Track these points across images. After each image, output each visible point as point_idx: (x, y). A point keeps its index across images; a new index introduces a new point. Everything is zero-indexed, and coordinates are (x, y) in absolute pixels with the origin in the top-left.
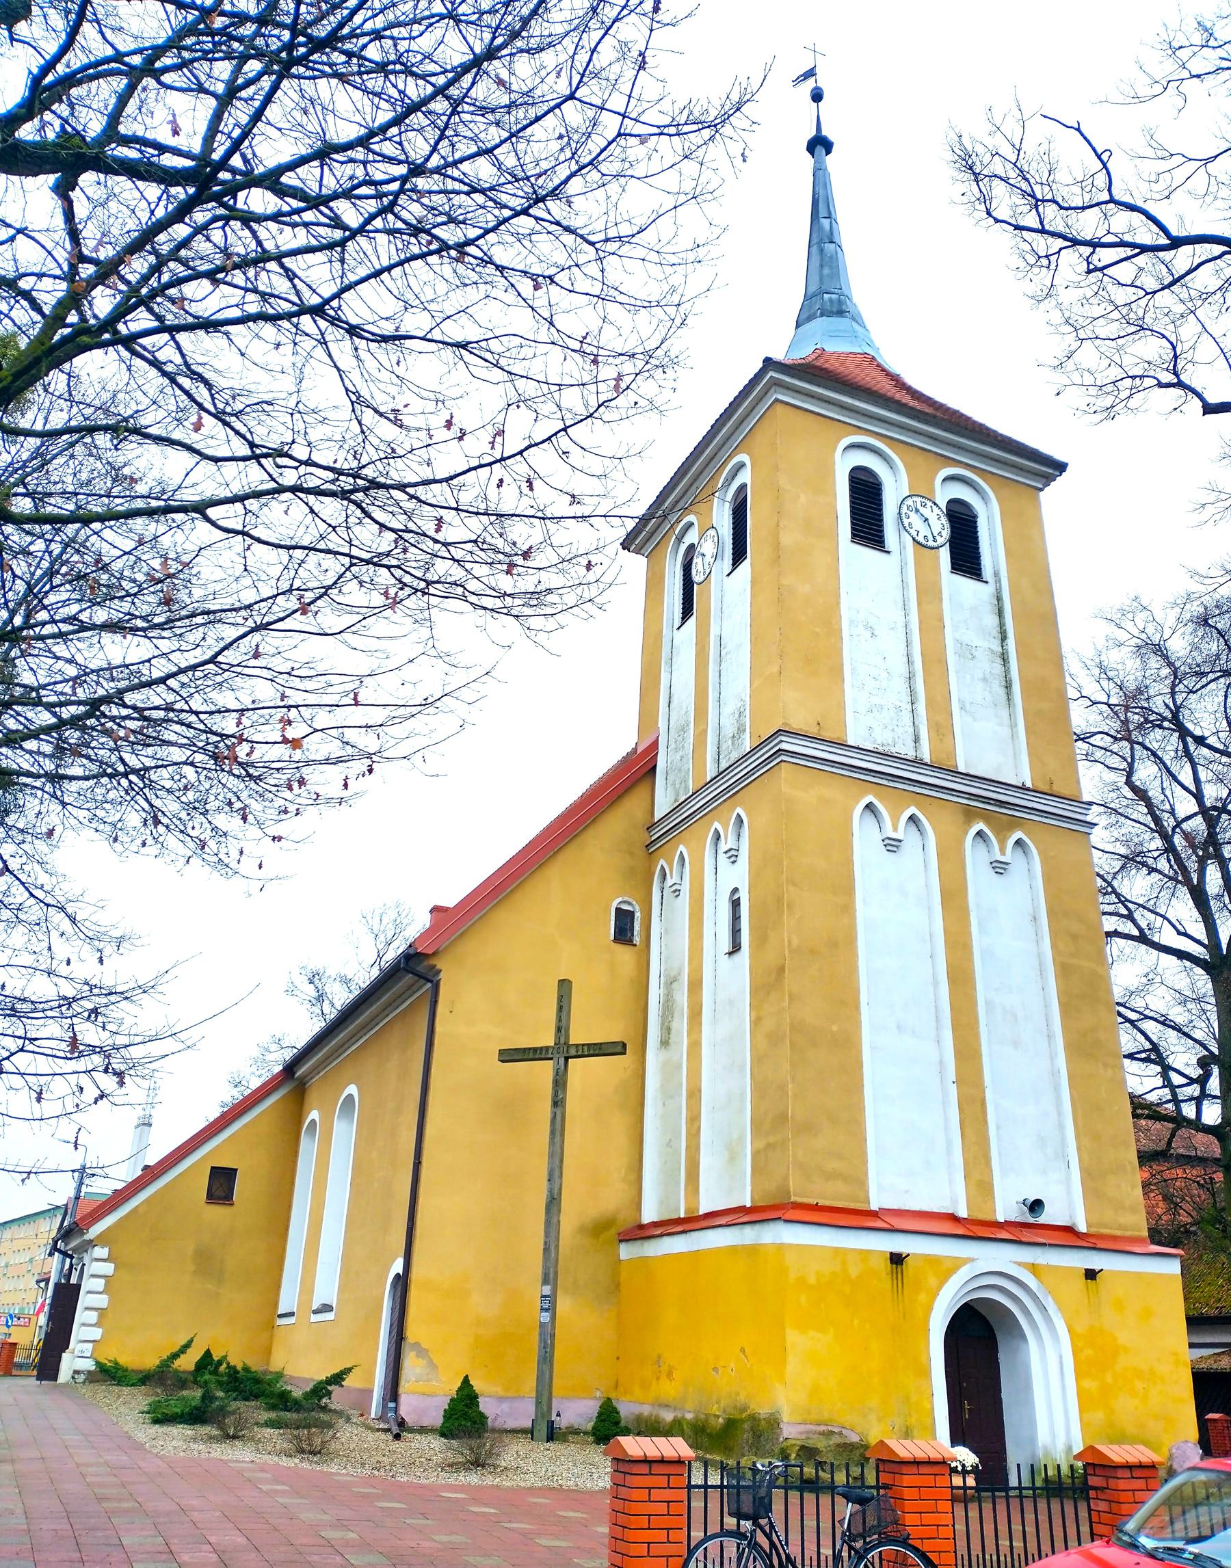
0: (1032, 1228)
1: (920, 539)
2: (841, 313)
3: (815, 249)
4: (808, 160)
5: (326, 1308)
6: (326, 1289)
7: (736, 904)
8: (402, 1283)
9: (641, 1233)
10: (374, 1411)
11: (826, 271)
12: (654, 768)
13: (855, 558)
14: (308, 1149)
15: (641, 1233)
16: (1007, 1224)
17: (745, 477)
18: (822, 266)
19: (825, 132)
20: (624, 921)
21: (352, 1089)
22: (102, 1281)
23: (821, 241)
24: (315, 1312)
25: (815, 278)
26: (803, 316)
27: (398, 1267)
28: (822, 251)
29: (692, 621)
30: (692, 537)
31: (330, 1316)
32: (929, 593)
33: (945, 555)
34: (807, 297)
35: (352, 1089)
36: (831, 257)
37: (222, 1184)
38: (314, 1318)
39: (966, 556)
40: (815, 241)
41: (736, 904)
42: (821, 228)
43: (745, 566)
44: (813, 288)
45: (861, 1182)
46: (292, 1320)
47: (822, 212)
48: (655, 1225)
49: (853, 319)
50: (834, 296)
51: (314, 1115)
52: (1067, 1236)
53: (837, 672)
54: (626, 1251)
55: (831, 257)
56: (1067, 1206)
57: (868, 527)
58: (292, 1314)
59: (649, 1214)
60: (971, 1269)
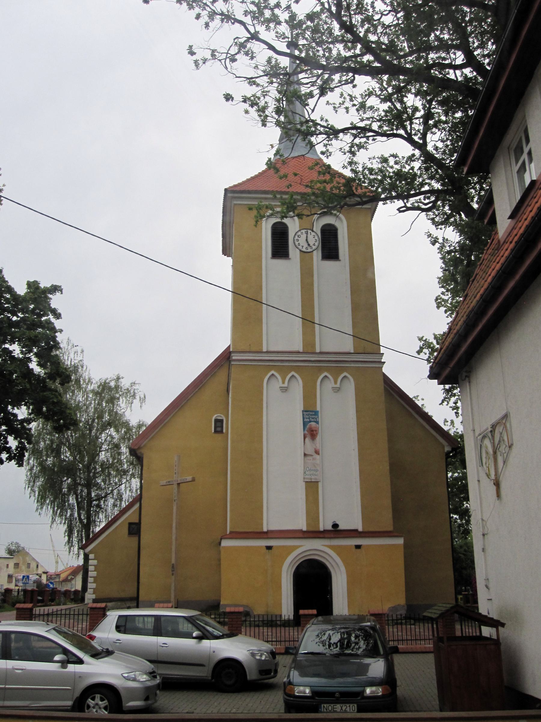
0: (335, 531)
1: (304, 250)
16: (325, 531)
20: (219, 423)
33: (317, 255)
52: (353, 533)
57: (280, 249)
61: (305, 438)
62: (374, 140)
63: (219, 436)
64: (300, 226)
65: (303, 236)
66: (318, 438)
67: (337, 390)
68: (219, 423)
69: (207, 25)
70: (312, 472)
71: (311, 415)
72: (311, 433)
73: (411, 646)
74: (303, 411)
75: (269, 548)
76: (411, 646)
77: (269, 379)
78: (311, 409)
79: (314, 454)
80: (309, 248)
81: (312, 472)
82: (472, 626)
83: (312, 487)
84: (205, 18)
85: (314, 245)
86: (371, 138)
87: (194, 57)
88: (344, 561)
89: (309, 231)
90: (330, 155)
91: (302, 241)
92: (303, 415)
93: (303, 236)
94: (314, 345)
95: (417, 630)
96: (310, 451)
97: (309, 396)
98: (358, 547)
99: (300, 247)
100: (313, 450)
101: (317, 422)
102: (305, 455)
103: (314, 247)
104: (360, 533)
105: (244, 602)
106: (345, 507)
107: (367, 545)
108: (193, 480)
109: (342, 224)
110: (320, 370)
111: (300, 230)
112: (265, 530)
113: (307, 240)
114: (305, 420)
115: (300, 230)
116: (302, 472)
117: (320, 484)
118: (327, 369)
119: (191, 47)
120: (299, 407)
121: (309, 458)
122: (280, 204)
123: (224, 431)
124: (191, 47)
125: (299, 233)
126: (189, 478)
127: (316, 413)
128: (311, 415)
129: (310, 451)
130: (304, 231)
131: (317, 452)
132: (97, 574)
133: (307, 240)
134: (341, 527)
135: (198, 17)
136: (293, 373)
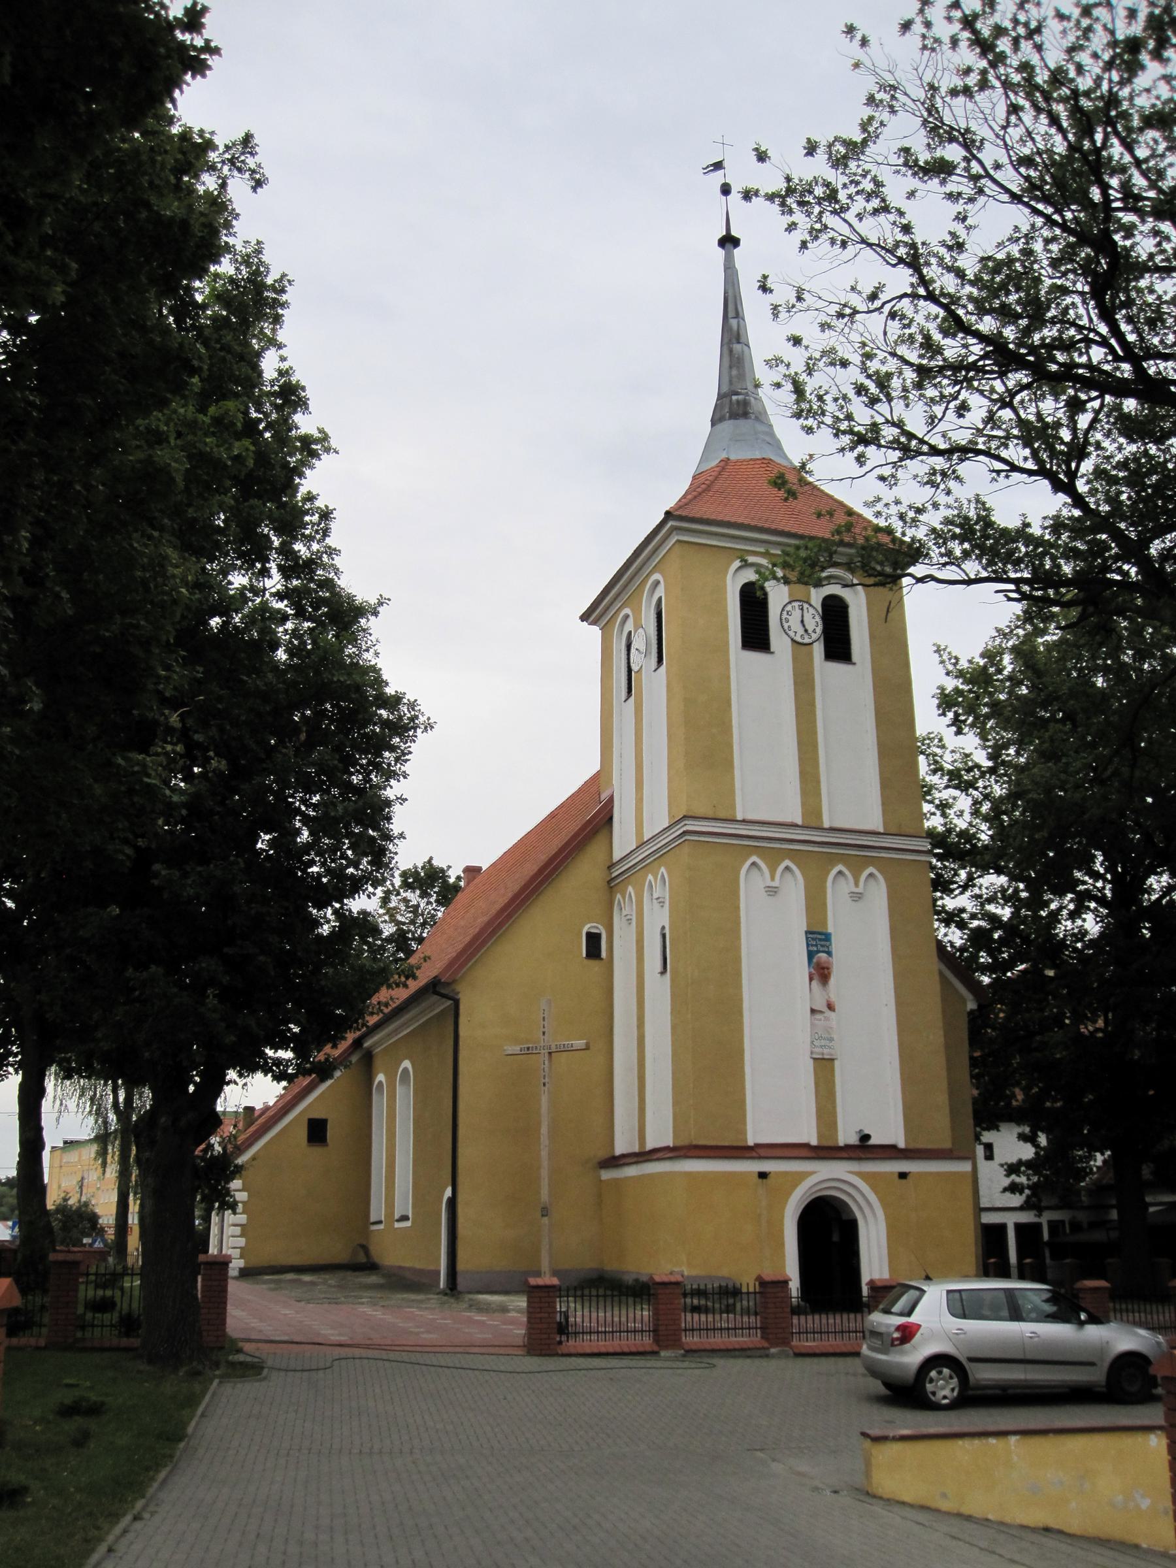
0: (863, 1149)
1: (798, 639)
2: (745, 415)
3: (725, 347)
4: (721, 253)
5: (404, 1218)
6: (404, 1202)
7: (664, 936)
8: (452, 1203)
9: (614, 1162)
10: (442, 1285)
11: (734, 372)
12: (611, 818)
13: (742, 661)
14: (380, 1104)
15: (614, 1162)
16: (848, 1147)
17: (660, 592)
18: (731, 367)
19: (734, 233)
20: (593, 940)
21: (407, 1064)
22: (239, 1228)
23: (730, 342)
24: (398, 1221)
25: (726, 380)
26: (717, 417)
27: (448, 1192)
28: (731, 351)
29: (632, 698)
30: (629, 626)
31: (408, 1224)
32: (804, 684)
33: (818, 650)
34: (721, 396)
35: (407, 1064)
36: (738, 358)
37: (317, 1131)
38: (397, 1225)
39: (838, 646)
40: (726, 340)
41: (664, 936)
42: (731, 329)
43: (663, 668)
44: (725, 389)
45: (744, 1132)
46: (381, 1227)
47: (731, 314)
48: (623, 1156)
49: (757, 419)
50: (740, 397)
51: (381, 1077)
52: (890, 1152)
53: (729, 764)
54: (606, 1175)
55: (738, 358)
56: (889, 1129)
57: (756, 636)
58: (380, 1222)
59: (618, 1151)
60: (822, 1176)
61: (811, 979)
62: (1007, 477)
63: (593, 963)
64: (790, 595)
65: (793, 614)
66: (832, 981)
67: (857, 897)
68: (593, 940)
69: (804, 245)
70: (823, 1042)
71: (820, 940)
72: (821, 973)
73: (826, 1343)
74: (807, 933)
75: (763, 1175)
76: (826, 1343)
77: (748, 871)
78: (820, 930)
79: (825, 1009)
80: (806, 637)
81: (823, 1042)
82: (1158, 1312)
83: (824, 1066)
84: (800, 235)
85: (814, 631)
86: (1003, 474)
87: (769, 298)
88: (881, 1200)
89: (806, 606)
90: (895, 484)
91: (794, 622)
92: (807, 938)
93: (793, 614)
94: (819, 815)
95: (624, 1319)
96: (820, 1005)
97: (815, 903)
98: (903, 1176)
99: (792, 634)
100: (825, 1003)
101: (829, 953)
102: (813, 1011)
103: (815, 636)
104: (816, 1148)
105: (725, 1272)
106: (876, 1105)
107: (918, 1173)
108: (587, 1048)
109: (858, 603)
110: (833, 859)
111: (790, 603)
112: (750, 1143)
113: (802, 621)
114: (811, 948)
115: (790, 603)
116: (809, 1040)
117: (836, 1063)
118: (756, 850)
119: (765, 277)
120: (799, 925)
121: (818, 1016)
122: (779, 552)
123: (604, 954)
124: (765, 277)
125: (789, 608)
126: (580, 1043)
127: (827, 937)
128: (820, 940)
129: (820, 1005)
130: (796, 604)
131: (831, 1007)
132: (248, 1219)
133: (802, 621)
134: (873, 1141)
135: (792, 227)
136: (754, 858)
